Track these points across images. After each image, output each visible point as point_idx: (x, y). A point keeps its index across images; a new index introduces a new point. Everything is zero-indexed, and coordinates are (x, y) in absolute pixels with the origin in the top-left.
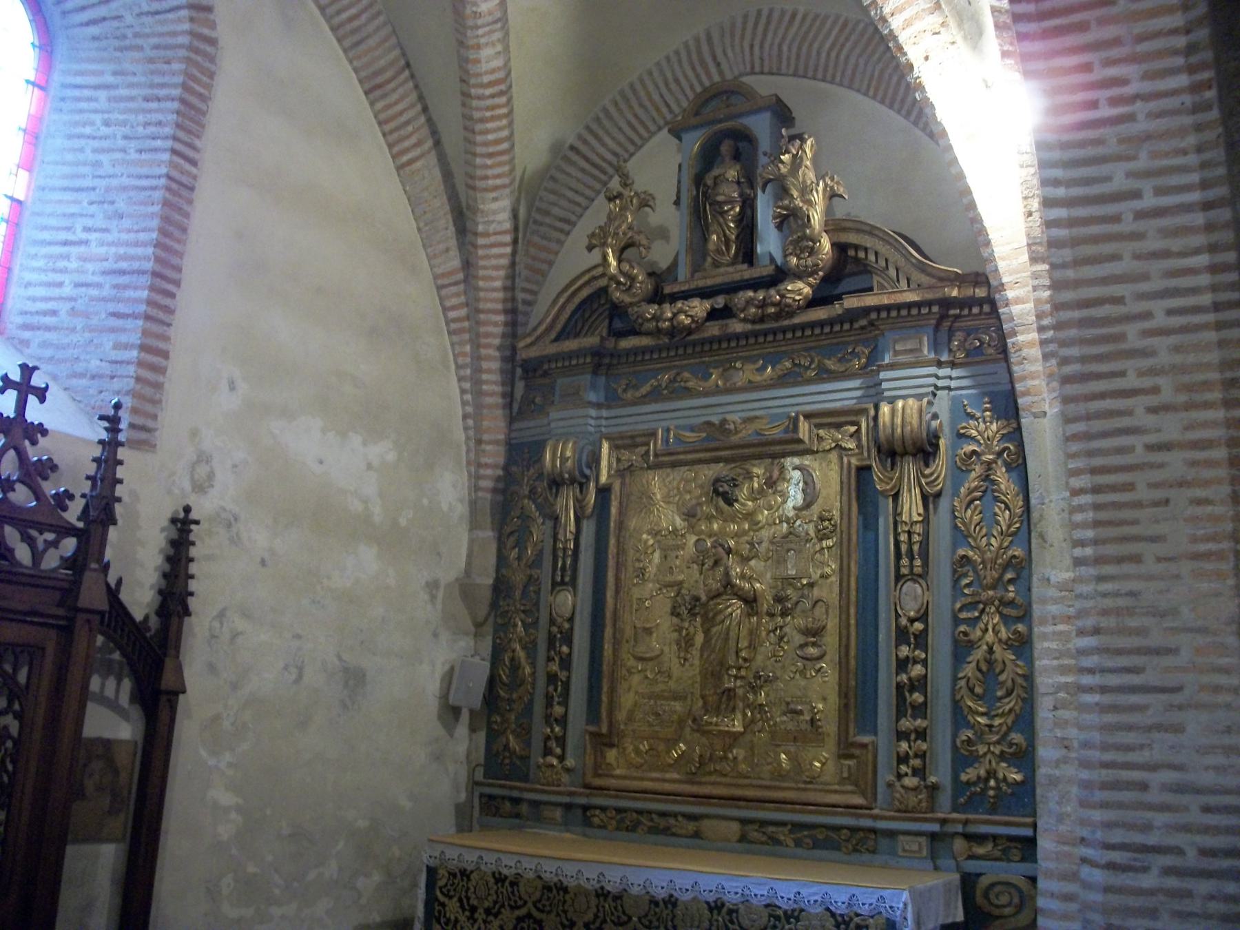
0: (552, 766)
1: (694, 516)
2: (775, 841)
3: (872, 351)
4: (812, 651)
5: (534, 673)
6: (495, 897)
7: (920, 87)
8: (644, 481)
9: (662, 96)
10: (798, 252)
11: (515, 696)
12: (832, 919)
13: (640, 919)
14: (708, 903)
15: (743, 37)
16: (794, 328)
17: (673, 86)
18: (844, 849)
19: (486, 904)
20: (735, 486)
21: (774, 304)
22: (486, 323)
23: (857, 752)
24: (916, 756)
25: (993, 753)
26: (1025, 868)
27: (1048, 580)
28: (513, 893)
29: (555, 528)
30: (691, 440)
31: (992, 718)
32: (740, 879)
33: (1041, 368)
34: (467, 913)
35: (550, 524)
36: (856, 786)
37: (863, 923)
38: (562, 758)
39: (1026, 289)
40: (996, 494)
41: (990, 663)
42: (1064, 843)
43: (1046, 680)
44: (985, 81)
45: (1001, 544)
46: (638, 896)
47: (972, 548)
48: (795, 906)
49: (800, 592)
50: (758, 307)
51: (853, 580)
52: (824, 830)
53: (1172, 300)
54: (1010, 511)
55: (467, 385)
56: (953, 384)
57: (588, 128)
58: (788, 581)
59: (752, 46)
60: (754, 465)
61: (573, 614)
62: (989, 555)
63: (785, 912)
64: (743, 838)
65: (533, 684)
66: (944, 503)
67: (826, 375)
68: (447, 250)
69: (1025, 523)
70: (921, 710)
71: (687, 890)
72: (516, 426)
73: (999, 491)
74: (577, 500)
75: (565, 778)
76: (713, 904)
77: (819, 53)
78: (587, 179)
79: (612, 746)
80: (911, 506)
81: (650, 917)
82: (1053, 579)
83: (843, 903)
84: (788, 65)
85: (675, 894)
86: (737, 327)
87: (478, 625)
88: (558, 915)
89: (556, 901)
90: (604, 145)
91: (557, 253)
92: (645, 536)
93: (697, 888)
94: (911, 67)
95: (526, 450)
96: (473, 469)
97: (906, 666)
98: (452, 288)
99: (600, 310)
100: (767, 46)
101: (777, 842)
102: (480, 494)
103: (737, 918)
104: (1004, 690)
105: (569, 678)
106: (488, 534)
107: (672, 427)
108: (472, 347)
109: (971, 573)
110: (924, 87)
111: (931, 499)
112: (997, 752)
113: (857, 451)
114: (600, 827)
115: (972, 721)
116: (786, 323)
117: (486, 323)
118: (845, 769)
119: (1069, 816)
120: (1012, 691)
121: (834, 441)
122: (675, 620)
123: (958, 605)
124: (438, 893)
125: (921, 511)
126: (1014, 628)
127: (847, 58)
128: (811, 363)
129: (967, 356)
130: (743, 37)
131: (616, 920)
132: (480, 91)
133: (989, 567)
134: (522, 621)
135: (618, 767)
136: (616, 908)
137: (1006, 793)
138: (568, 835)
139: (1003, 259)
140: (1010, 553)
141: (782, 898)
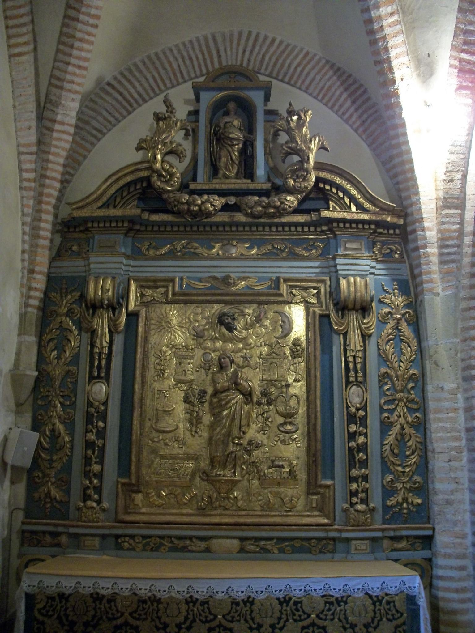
0: (93, 508)
1: (202, 337)
2: (265, 550)
3: (325, 246)
4: (289, 427)
5: (72, 442)
6: (93, 612)
7: (397, 95)
8: (163, 311)
9: (179, 66)
10: (295, 177)
11: (55, 457)
12: (370, 600)
13: (224, 616)
14: (278, 599)
15: (238, 44)
16: (283, 225)
17: (188, 62)
18: (313, 552)
19: (85, 619)
20: (234, 319)
21: (275, 207)
22: (50, 187)
23: (322, 490)
24: (363, 491)
25: (406, 488)
26: (426, 554)
27: (442, 388)
28: (110, 608)
29: (92, 338)
30: (200, 287)
31: (404, 467)
32: (303, 580)
33: (437, 269)
34: (66, 628)
35: (86, 337)
36: (321, 512)
37: (391, 600)
38: (99, 502)
39: (433, 223)
40: (402, 338)
41: (402, 435)
42: (458, 538)
43: (442, 445)
44: (425, 103)
45: (406, 367)
46: (222, 600)
47: (389, 368)
48: (344, 594)
49: (280, 391)
50: (264, 207)
51: (318, 384)
52: (300, 541)
53: (253, 262)
54: (410, 348)
55: (27, 229)
56: (377, 272)
57: (121, 73)
58: (272, 383)
59: (244, 51)
60: (246, 308)
61: (107, 399)
62: (399, 373)
63: (337, 599)
64: (242, 550)
65: (72, 449)
66: (373, 340)
67: (294, 256)
68: (29, 128)
69: (419, 356)
70: (364, 464)
71: (262, 592)
72: (57, 264)
73: (404, 336)
74: (109, 319)
75: (102, 516)
76: (282, 600)
77: (289, 66)
78: (118, 106)
79: (139, 492)
80: (355, 340)
81: (232, 614)
82: (446, 388)
83: (378, 588)
84: (266, 69)
85: (252, 595)
86: (241, 218)
87: (19, 405)
88: (152, 620)
89: (59, 608)
90: (134, 87)
91: (89, 151)
92: (164, 348)
93: (270, 590)
94: (394, 82)
95: (65, 282)
96: (24, 291)
97: (355, 437)
98: (28, 156)
99: (135, 193)
100: (255, 54)
101: (268, 551)
102: (29, 309)
103: (301, 607)
104: (411, 450)
105: (104, 445)
106: (32, 339)
107: (185, 277)
108: (34, 202)
109: (389, 383)
110: (399, 96)
111: (367, 337)
112: (408, 487)
113: (317, 305)
114: (128, 549)
115: (393, 470)
116: (276, 220)
117: (50, 187)
118: (314, 502)
119: (460, 521)
120: (415, 451)
121: (302, 297)
122: (187, 406)
123: (383, 401)
124: (36, 612)
125: (362, 344)
126: (414, 415)
127: (308, 73)
128: (285, 248)
129: (383, 257)
130: (238, 44)
131: (204, 620)
132: (86, 18)
133: (400, 380)
134: (60, 403)
135: (143, 507)
136: (203, 611)
137: (412, 511)
138: (105, 557)
139: (424, 204)
140: (411, 372)
141: (334, 589)
